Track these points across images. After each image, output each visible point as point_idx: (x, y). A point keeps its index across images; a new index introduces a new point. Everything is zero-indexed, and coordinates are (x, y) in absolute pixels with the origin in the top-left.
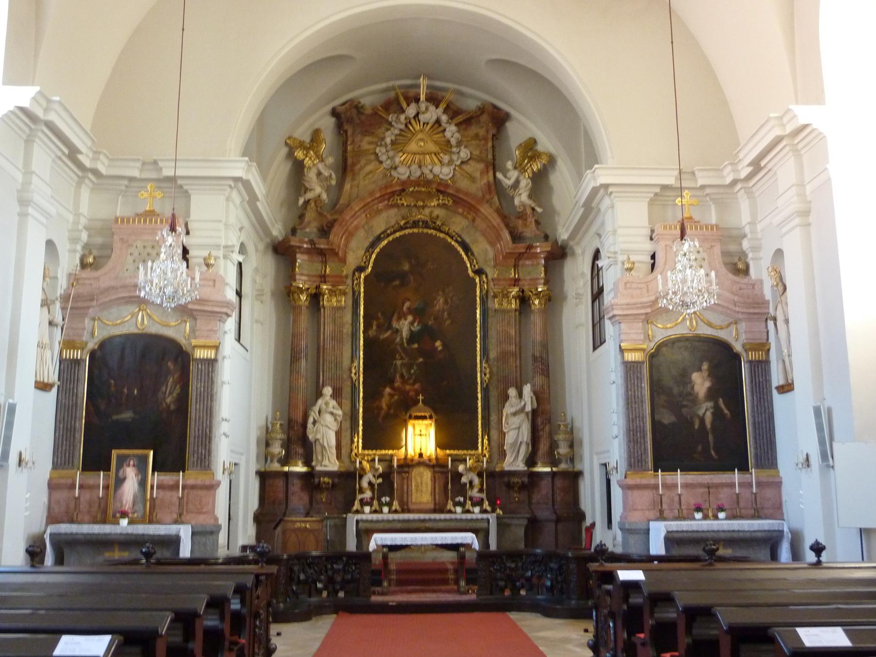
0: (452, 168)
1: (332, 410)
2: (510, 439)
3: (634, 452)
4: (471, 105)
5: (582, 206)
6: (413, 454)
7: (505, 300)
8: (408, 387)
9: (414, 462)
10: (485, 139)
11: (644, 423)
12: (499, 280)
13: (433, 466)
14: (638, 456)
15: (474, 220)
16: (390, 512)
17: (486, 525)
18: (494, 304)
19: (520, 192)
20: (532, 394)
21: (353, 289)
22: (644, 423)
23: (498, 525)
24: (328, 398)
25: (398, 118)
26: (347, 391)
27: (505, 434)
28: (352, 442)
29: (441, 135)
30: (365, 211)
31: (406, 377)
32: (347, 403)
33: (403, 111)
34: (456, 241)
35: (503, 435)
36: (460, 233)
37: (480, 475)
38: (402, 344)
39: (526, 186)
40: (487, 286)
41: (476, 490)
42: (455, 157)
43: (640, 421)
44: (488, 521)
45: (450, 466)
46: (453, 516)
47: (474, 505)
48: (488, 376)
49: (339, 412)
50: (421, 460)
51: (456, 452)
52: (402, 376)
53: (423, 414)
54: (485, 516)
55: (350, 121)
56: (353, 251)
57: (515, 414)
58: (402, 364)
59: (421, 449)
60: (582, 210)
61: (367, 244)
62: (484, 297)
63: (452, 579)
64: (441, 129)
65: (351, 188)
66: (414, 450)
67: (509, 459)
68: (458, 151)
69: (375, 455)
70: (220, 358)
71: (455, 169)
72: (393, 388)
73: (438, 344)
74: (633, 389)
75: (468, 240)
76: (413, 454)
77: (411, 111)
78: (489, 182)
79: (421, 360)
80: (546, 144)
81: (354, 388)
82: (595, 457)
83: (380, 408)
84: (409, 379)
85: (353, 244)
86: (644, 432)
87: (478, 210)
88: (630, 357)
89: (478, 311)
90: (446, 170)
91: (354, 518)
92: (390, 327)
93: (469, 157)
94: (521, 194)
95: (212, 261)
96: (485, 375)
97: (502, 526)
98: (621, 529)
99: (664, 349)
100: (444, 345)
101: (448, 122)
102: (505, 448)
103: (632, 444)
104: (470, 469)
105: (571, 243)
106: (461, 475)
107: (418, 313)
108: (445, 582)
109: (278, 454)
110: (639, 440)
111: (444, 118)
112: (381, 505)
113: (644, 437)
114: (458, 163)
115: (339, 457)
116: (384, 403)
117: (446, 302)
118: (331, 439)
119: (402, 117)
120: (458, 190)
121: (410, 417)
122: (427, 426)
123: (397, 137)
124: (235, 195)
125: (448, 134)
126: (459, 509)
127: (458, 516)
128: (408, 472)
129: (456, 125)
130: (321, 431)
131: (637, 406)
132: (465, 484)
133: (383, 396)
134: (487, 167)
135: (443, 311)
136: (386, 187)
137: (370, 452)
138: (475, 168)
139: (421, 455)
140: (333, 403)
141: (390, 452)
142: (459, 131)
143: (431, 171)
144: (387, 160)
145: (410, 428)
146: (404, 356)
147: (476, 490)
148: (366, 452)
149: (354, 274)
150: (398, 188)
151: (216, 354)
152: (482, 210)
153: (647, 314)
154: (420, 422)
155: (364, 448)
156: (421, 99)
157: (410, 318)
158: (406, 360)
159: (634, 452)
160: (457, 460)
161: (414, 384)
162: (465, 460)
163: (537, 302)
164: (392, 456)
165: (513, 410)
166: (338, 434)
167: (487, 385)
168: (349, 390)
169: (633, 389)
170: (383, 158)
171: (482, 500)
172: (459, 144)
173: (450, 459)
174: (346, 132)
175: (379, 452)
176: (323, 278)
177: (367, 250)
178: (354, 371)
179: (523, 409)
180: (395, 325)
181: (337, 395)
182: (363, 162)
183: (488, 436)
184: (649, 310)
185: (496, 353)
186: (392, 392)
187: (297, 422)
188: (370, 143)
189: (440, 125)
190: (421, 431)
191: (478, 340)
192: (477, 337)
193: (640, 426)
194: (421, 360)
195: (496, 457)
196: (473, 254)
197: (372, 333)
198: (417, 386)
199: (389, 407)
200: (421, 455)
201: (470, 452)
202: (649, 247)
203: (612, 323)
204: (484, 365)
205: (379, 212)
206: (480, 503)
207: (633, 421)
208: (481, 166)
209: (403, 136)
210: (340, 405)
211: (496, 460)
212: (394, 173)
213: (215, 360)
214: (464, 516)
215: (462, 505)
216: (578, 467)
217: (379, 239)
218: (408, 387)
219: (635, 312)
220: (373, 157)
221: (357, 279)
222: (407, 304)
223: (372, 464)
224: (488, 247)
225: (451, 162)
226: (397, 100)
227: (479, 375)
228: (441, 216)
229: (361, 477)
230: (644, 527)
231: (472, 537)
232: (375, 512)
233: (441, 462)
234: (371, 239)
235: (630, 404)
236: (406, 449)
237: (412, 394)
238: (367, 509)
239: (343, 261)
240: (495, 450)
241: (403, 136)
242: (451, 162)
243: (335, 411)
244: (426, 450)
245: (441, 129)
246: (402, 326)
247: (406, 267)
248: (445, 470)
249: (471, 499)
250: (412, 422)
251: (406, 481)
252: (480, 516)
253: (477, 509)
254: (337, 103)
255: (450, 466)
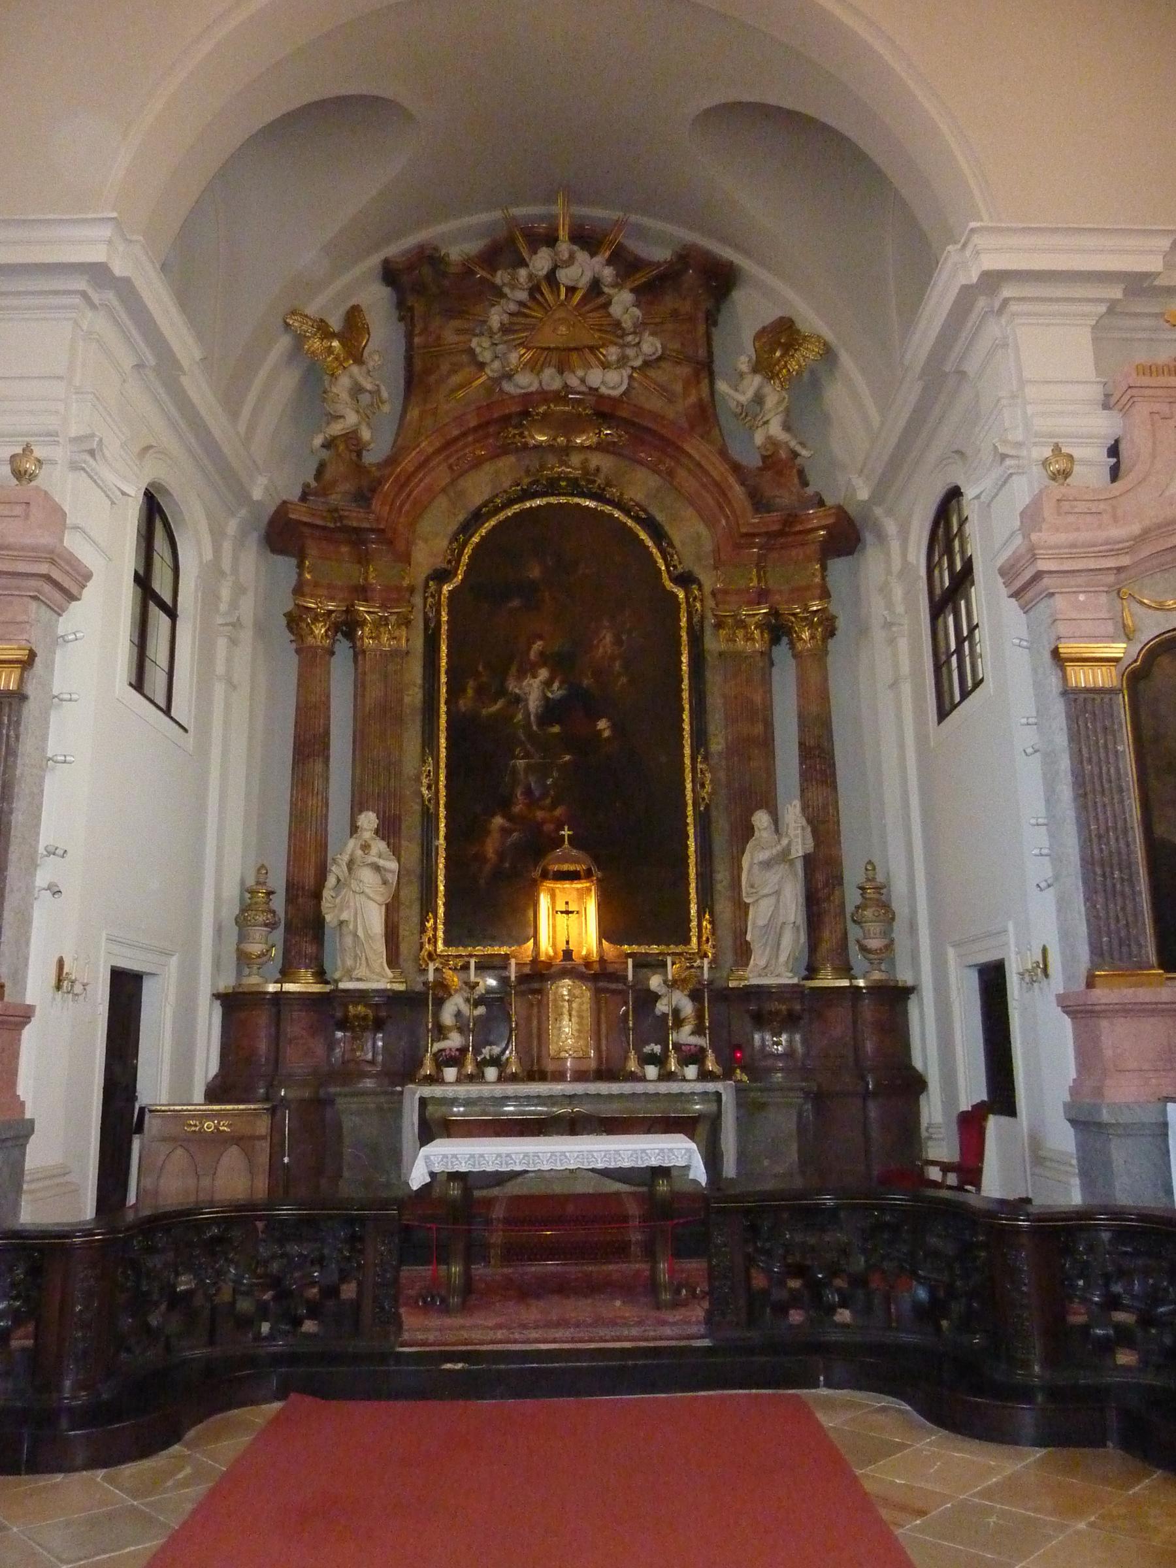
0: (626, 372)
1: (376, 859)
2: (759, 915)
3: (1108, 918)
4: (661, 254)
5: (920, 378)
6: (551, 953)
7: (740, 633)
8: (540, 814)
9: (553, 970)
10: (691, 319)
11: (1128, 845)
12: (725, 592)
13: (595, 978)
14: (1118, 931)
15: (671, 473)
16: (500, 1079)
17: (713, 1107)
18: (713, 644)
19: (765, 419)
20: (804, 822)
21: (425, 613)
22: (1128, 845)
23: (739, 1105)
24: (367, 835)
25: (514, 277)
26: (411, 823)
27: (747, 906)
28: (423, 930)
29: (602, 312)
30: (448, 457)
31: (537, 794)
32: (411, 850)
33: (523, 263)
34: (637, 519)
35: (742, 909)
36: (645, 503)
37: (695, 996)
38: (528, 724)
39: (779, 403)
40: (702, 606)
41: (687, 1029)
42: (630, 352)
43: (1117, 839)
44: (718, 1095)
45: (630, 977)
46: (639, 1088)
47: (685, 1061)
48: (708, 788)
49: (393, 865)
50: (568, 964)
51: (643, 949)
52: (528, 792)
53: (572, 868)
54: (711, 1087)
55: (420, 289)
56: (426, 541)
57: (767, 865)
58: (529, 768)
59: (568, 942)
60: (918, 387)
61: (453, 527)
62: (697, 628)
63: (637, 1242)
64: (602, 300)
65: (421, 417)
66: (554, 946)
67: (758, 959)
68: (637, 340)
69: (471, 956)
70: (30, 689)
71: (630, 377)
72: (509, 817)
73: (602, 724)
74: (1095, 759)
75: (660, 517)
76: (551, 953)
77: (541, 262)
78: (701, 400)
79: (567, 758)
80: (810, 320)
81: (429, 819)
82: (951, 953)
83: (480, 858)
84: (544, 795)
85: (426, 525)
86: (1127, 866)
87: (679, 449)
88: (1081, 677)
89: (685, 659)
90: (613, 377)
91: (414, 1094)
92: (502, 692)
93: (660, 352)
94: (766, 422)
95: (30, 466)
96: (703, 786)
97: (749, 1108)
98: (1073, 1122)
99: (1164, 661)
100: (614, 727)
101: (614, 285)
102: (748, 938)
103: (1100, 899)
104: (673, 985)
105: (878, 511)
106: (656, 997)
107: (560, 663)
108: (620, 1251)
109: (259, 957)
110: (1118, 886)
111: (608, 273)
112: (481, 1065)
113: (1131, 881)
114: (638, 363)
115: (393, 960)
116: (490, 848)
117: (618, 642)
118: (374, 920)
119: (523, 273)
120: (640, 411)
121: (545, 876)
122: (582, 894)
123: (515, 319)
124: (99, 323)
125: (616, 310)
126: (652, 1071)
127: (651, 1088)
128: (539, 991)
129: (632, 290)
130: (352, 904)
131: (1106, 800)
132: (665, 1015)
133: (488, 832)
134: (697, 374)
135: (612, 658)
136: (489, 406)
137: (462, 951)
138: (674, 375)
139: (568, 954)
140: (380, 846)
141: (504, 950)
142: (637, 304)
143: (583, 381)
144: (492, 361)
145: (544, 901)
146: (532, 750)
147: (687, 1029)
148: (452, 951)
149: (427, 586)
150: (515, 409)
151: (21, 681)
152: (687, 447)
153: (1119, 570)
154: (567, 885)
155: (447, 943)
156: (561, 237)
157: (544, 673)
158: (536, 760)
159: (1108, 918)
160: (645, 964)
161: (553, 807)
162: (664, 965)
163: (806, 635)
164: (507, 957)
165: (763, 856)
166: (392, 910)
167: (707, 807)
168: (417, 818)
169: (1095, 759)
170: (486, 356)
171: (702, 1050)
172: (639, 328)
173: (630, 961)
174: (411, 309)
175: (479, 950)
176: (362, 592)
177: (454, 538)
178: (425, 781)
179: (784, 856)
180: (512, 686)
181: (388, 830)
182: (445, 367)
183: (711, 915)
184: (1125, 561)
185: (722, 741)
186: (507, 825)
187: (303, 888)
188: (459, 332)
189: (600, 293)
190: (567, 903)
191: (686, 716)
192: (683, 710)
193: (1120, 853)
194: (567, 758)
195: (729, 958)
196: (671, 545)
197: (463, 704)
198: (558, 812)
199: (501, 856)
200: (568, 954)
201: (673, 948)
202: (1105, 425)
203: (1022, 607)
204: (699, 766)
205: (477, 464)
206: (695, 1057)
207: (1100, 837)
208: (685, 370)
209: (526, 316)
210: (396, 851)
211: (728, 965)
212: (508, 387)
213: (19, 697)
214: (664, 1088)
215: (659, 1060)
216: (905, 977)
217: (477, 517)
218: (540, 814)
219: (1093, 564)
220: (465, 358)
221: (433, 596)
222: (538, 646)
223: (463, 975)
224: (702, 529)
225: (623, 361)
226: (511, 241)
227: (689, 786)
228: (604, 470)
229: (439, 1003)
230: (1149, 1116)
231: (688, 1150)
232: (471, 1079)
233: (610, 969)
234: (461, 518)
235: (1090, 796)
236: (536, 944)
237: (549, 827)
238: (450, 1073)
239: (405, 558)
240: (728, 942)
241: (526, 316)
242: (623, 361)
243: (381, 862)
244: (580, 945)
245: (602, 300)
246: (527, 690)
247: (535, 573)
248: (620, 986)
249: (677, 1047)
250: (549, 884)
251: (535, 1010)
252: (699, 1087)
253: (691, 1071)
254: (392, 250)
255: (630, 977)
